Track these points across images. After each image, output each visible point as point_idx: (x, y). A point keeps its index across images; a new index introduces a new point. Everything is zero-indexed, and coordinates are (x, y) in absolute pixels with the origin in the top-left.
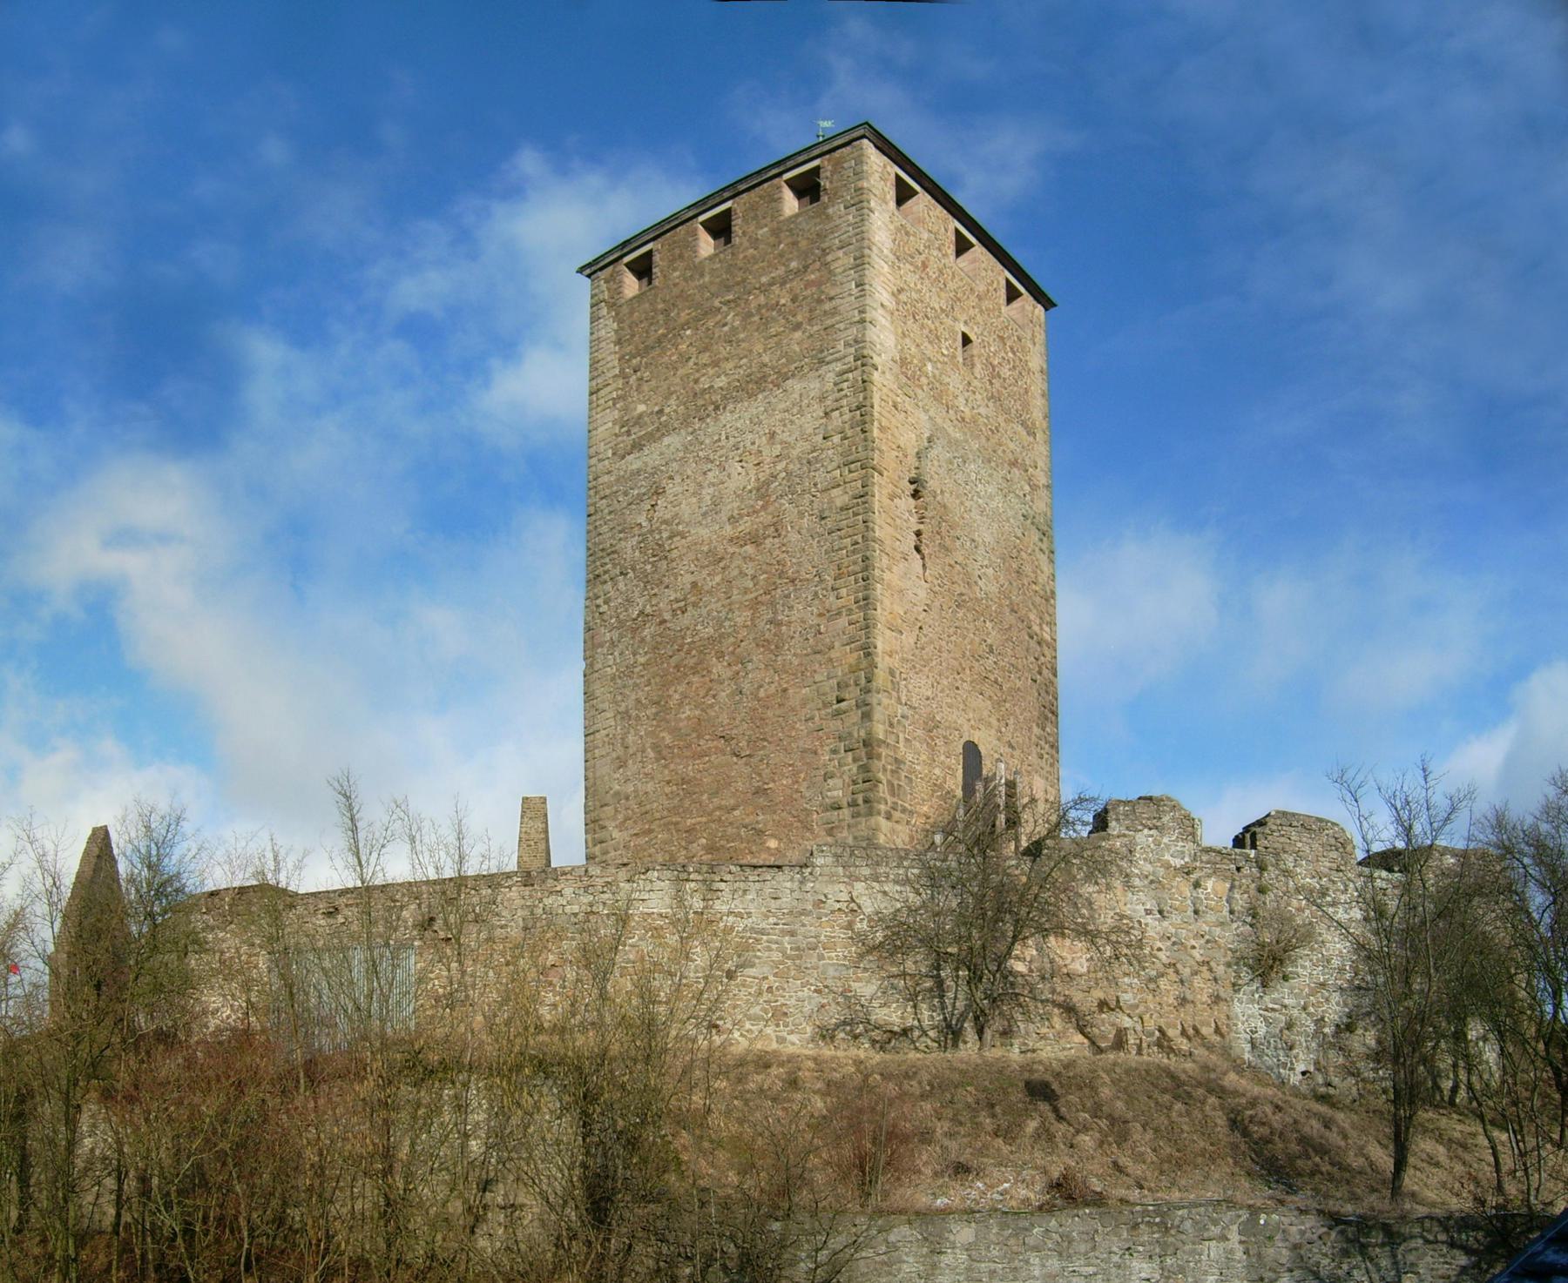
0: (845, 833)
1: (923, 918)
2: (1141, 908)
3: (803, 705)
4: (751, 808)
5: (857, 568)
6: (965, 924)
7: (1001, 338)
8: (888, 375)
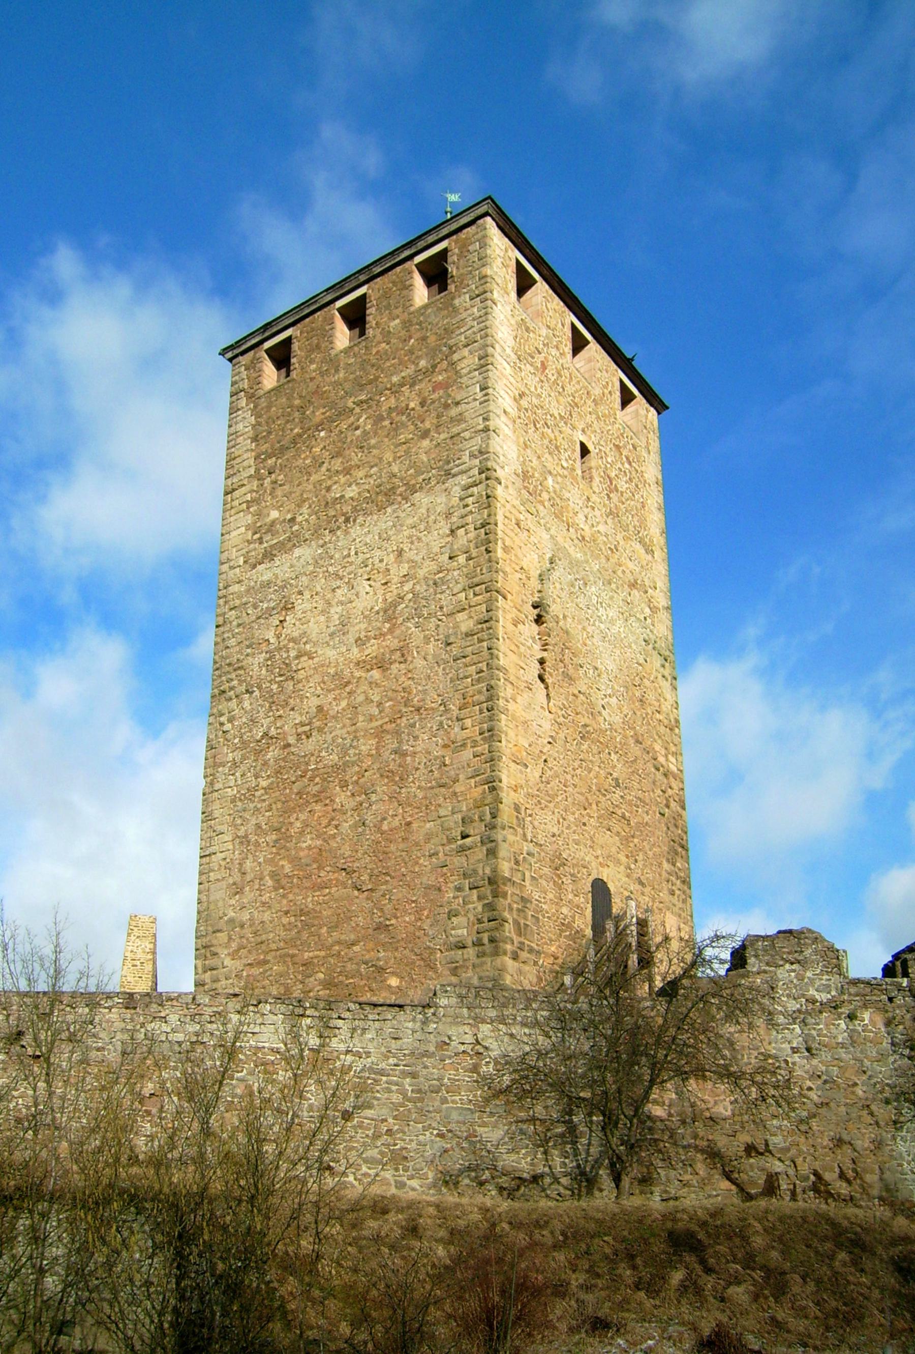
0: (470, 973)
1: (552, 1061)
2: (786, 1046)
3: (428, 840)
4: (371, 945)
5: (483, 698)
6: (599, 1068)
7: (617, 447)
8: (511, 491)
